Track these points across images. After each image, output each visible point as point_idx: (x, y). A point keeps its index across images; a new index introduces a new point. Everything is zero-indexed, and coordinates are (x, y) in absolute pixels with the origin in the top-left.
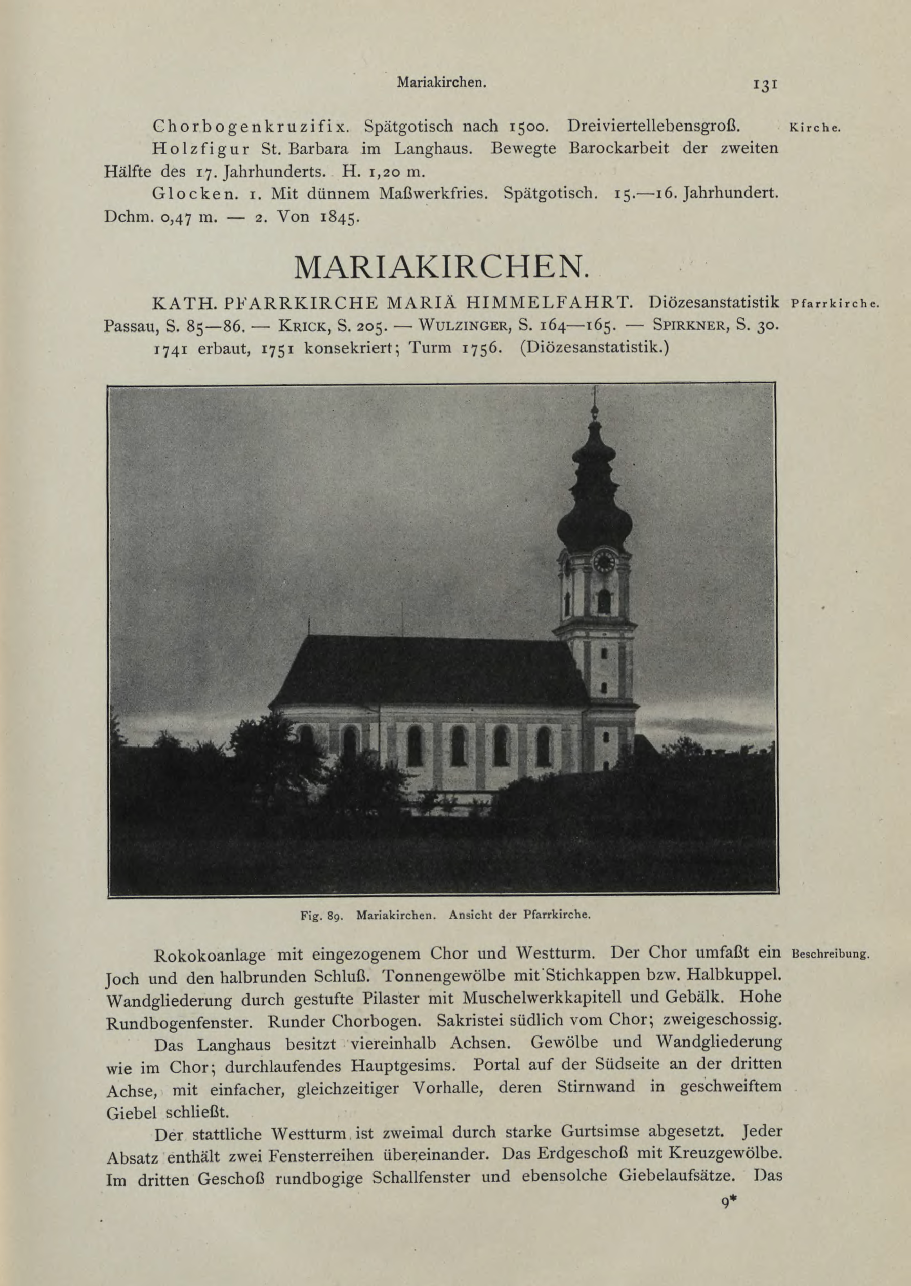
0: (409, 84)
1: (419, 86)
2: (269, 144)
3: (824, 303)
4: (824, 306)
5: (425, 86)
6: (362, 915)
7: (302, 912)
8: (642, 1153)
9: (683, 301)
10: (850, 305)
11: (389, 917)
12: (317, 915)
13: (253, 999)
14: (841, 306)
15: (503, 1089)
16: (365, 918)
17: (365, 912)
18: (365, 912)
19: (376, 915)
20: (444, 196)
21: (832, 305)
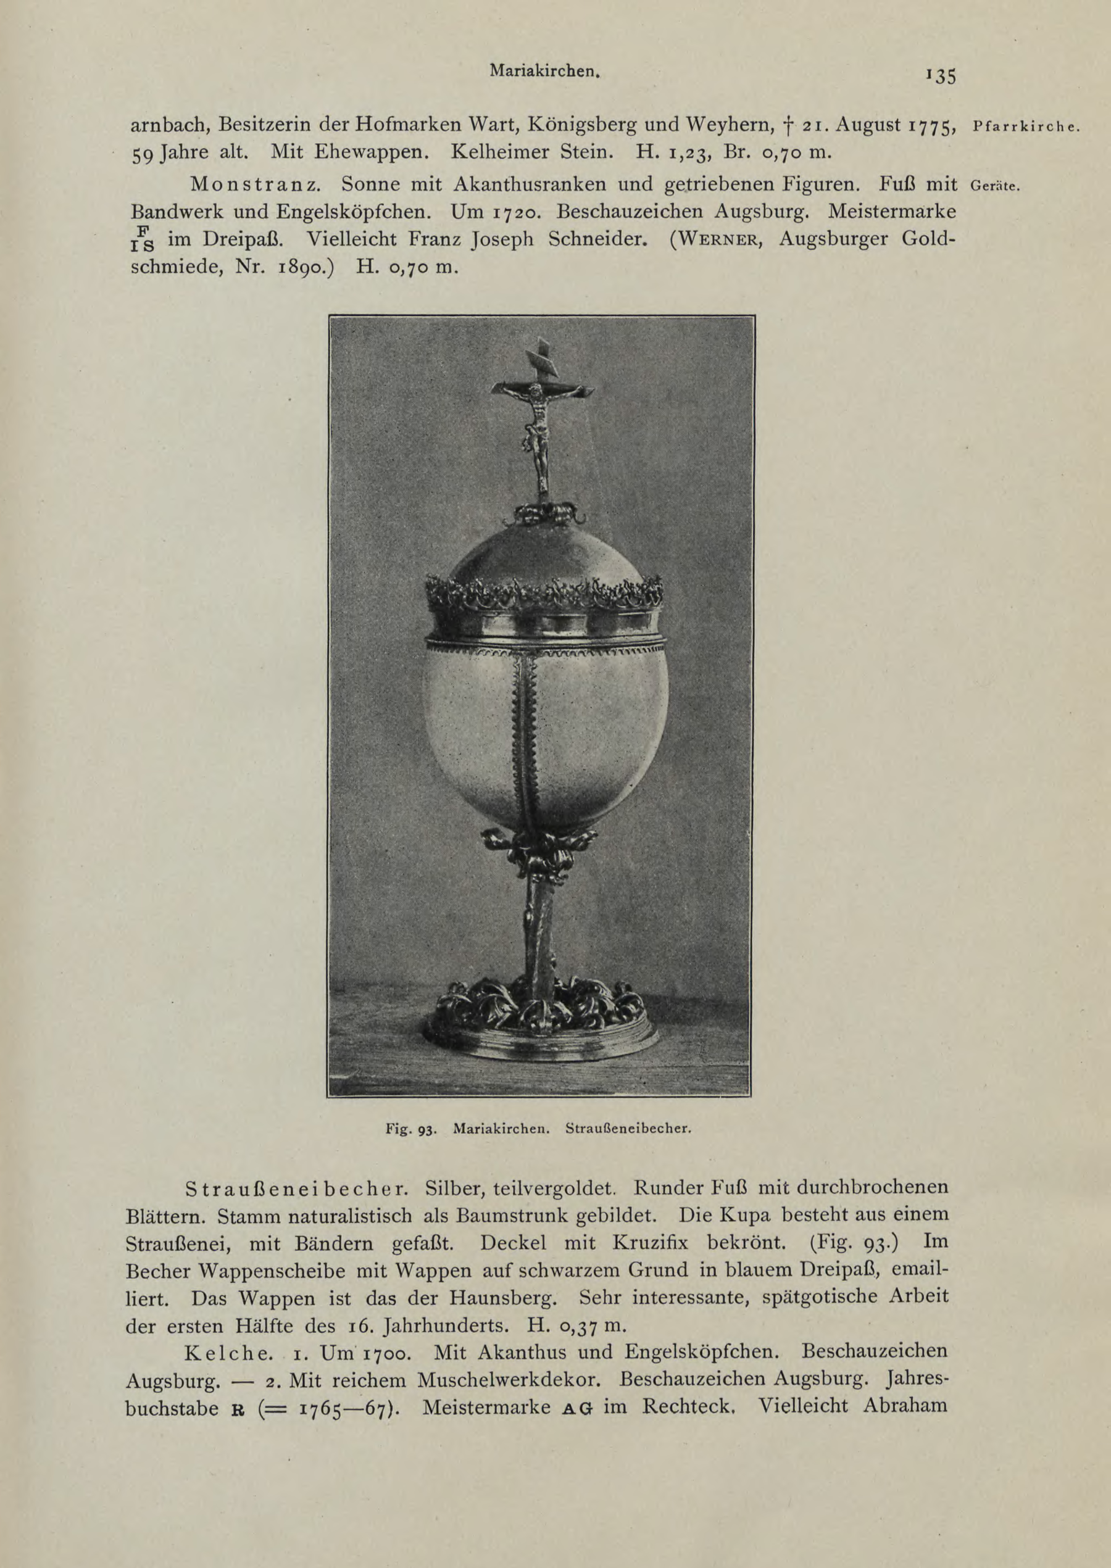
0: (505, 72)
1: (517, 75)
4: (1014, 130)
5: (524, 75)
10: (1044, 128)
11: (493, 1130)
12: (405, 1128)
13: (812, 1186)
14: (1033, 130)
21: (1024, 129)
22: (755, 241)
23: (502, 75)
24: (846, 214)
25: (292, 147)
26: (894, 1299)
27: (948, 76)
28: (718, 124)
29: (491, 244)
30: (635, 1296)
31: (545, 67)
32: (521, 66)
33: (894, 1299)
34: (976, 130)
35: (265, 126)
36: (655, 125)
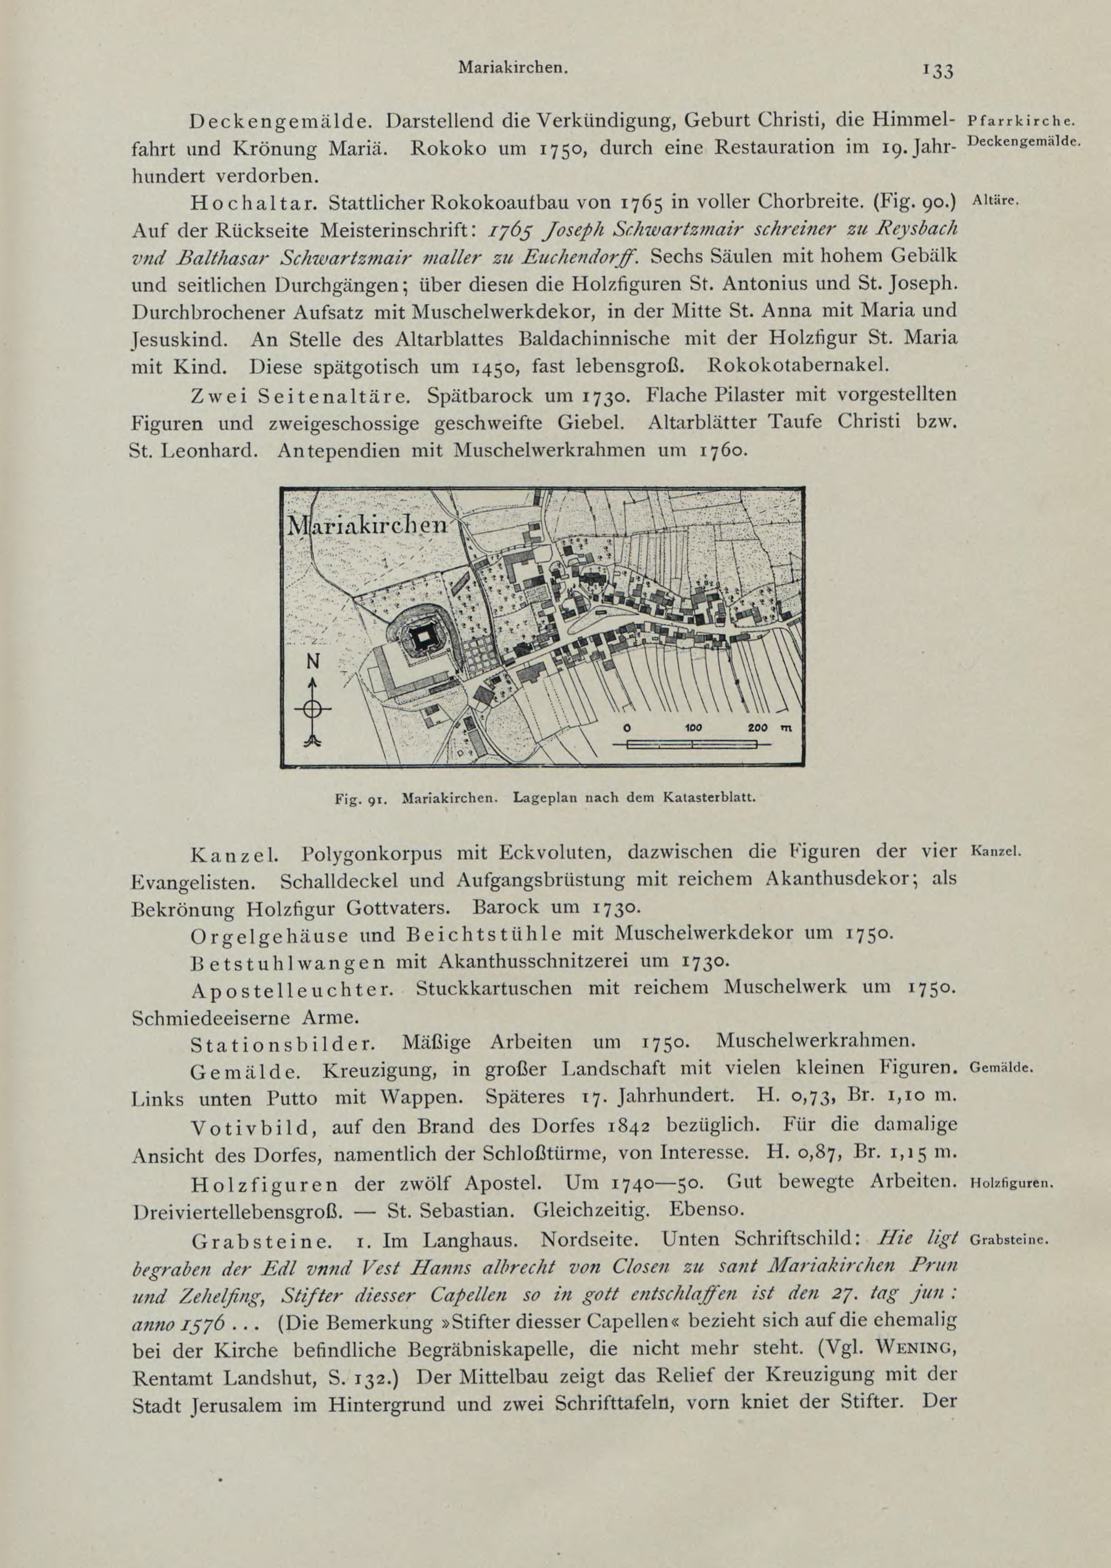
0: (473, 69)
4: (1009, 124)
5: (492, 72)
8: (828, 311)
10: (1040, 123)
11: (440, 800)
14: (1028, 124)
15: (358, 341)
19: (424, 798)
22: (226, 231)
23: (470, 72)
24: (338, 234)
25: (481, 1373)
29: (909, 287)
31: (513, 64)
32: (490, 64)
34: (970, 124)
35: (584, 963)
36: (602, 880)
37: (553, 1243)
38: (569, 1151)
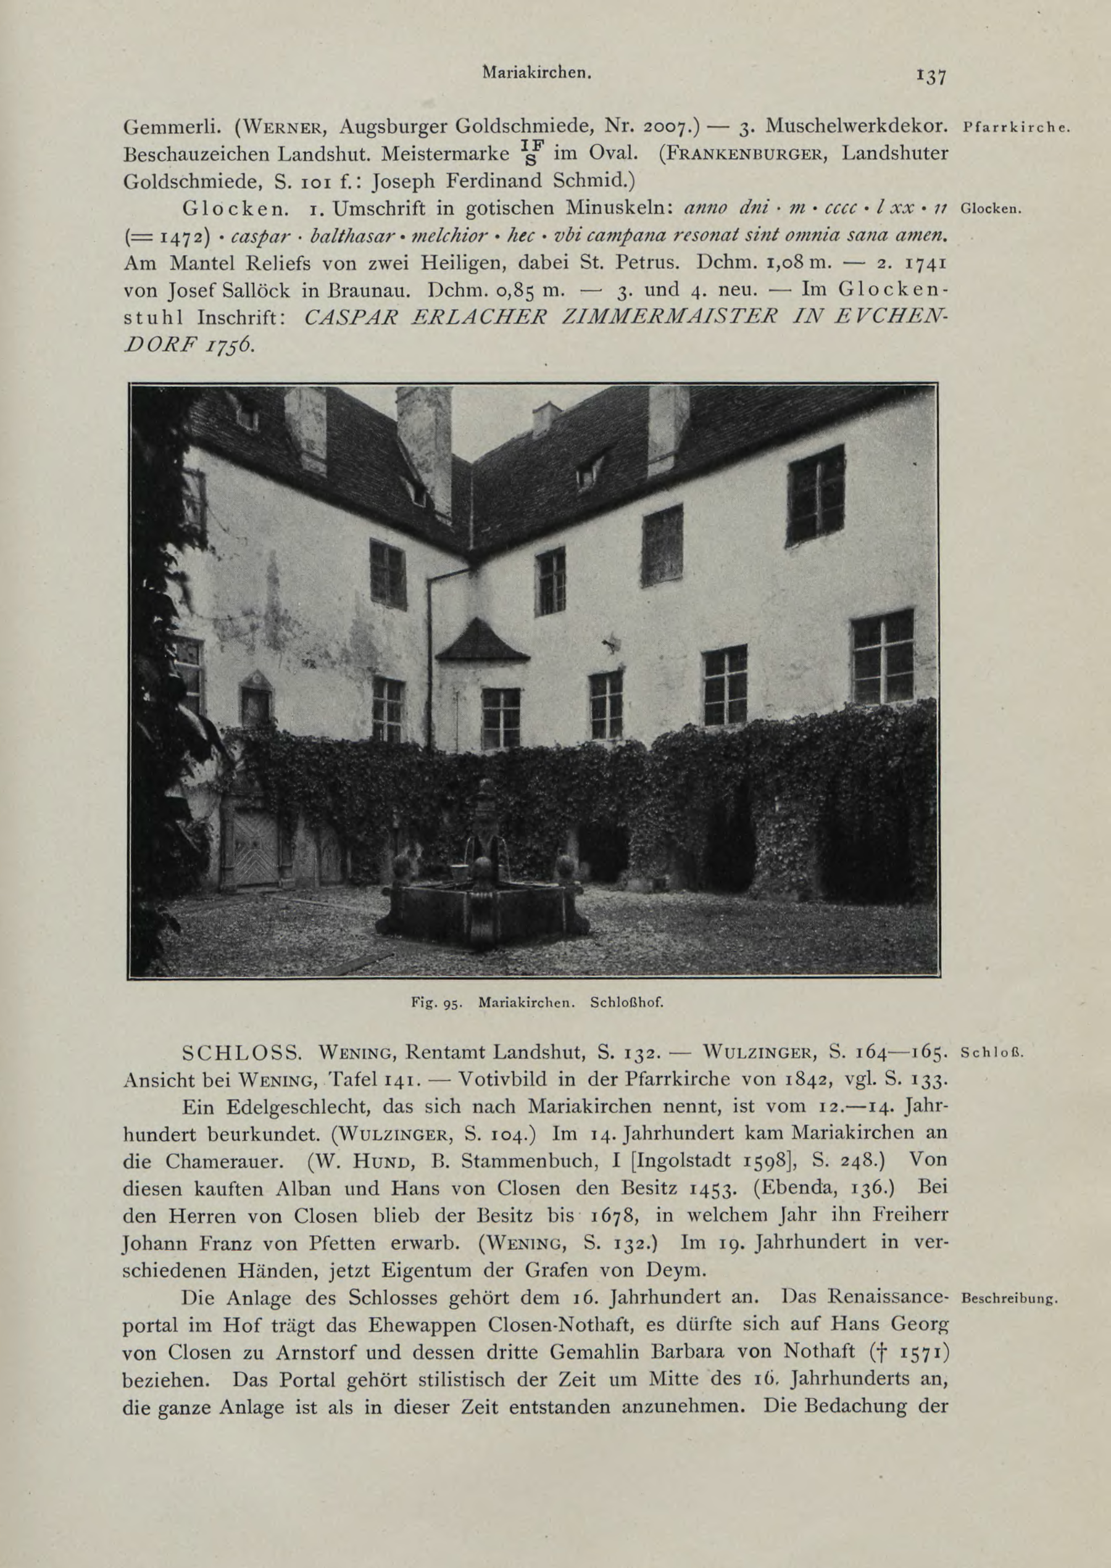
0: (497, 74)
2: (589, 256)
3: (1003, 127)
4: (1003, 130)
5: (516, 77)
6: (485, 1002)
7: (414, 998)
9: (207, 152)
10: (1034, 129)
11: (517, 1004)
12: (431, 1001)
14: (1023, 131)
16: (489, 1006)
17: (489, 999)
18: (489, 999)
20: (1013, 130)
24: (399, 156)
26: (281, 1357)
27: (937, 77)
28: (674, 1270)
30: (439, 207)
33: (281, 1357)
34: (966, 130)
37: (796, 1354)
38: (703, 1322)
